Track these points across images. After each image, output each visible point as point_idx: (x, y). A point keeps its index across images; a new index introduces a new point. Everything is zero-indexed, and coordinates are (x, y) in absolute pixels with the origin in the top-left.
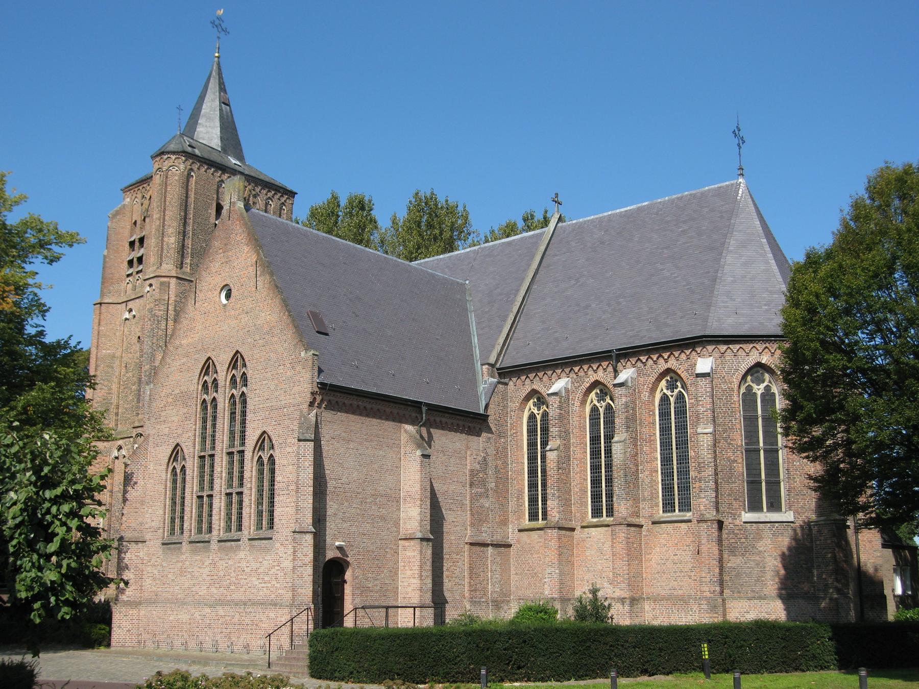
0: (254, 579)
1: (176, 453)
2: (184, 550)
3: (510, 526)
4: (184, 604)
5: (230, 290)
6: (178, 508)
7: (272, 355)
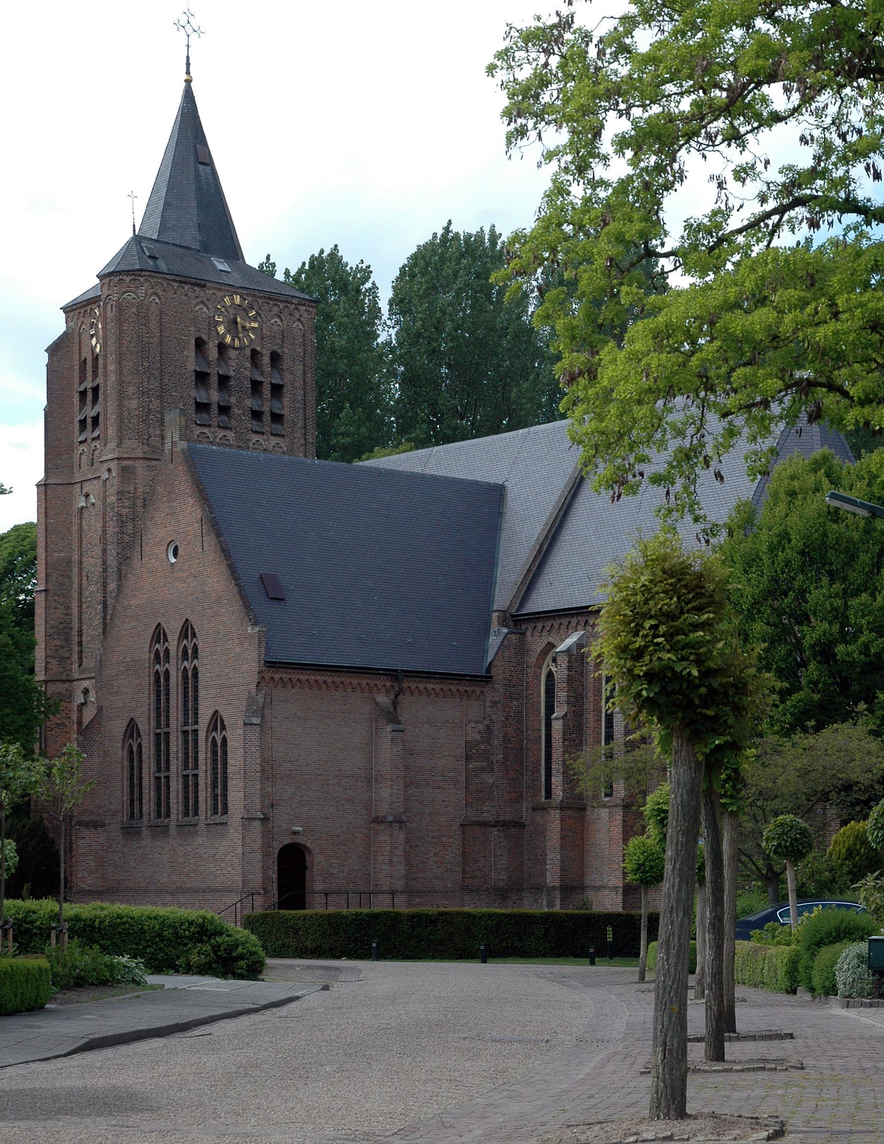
0: (211, 865)
1: (132, 729)
2: (144, 834)
3: (525, 804)
4: (146, 892)
5: (176, 546)
6: (136, 790)
7: (221, 627)
